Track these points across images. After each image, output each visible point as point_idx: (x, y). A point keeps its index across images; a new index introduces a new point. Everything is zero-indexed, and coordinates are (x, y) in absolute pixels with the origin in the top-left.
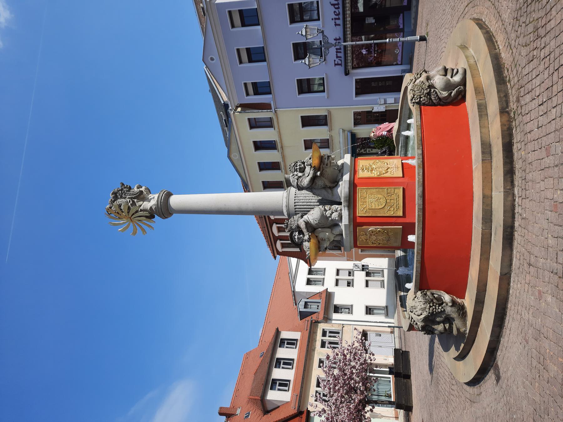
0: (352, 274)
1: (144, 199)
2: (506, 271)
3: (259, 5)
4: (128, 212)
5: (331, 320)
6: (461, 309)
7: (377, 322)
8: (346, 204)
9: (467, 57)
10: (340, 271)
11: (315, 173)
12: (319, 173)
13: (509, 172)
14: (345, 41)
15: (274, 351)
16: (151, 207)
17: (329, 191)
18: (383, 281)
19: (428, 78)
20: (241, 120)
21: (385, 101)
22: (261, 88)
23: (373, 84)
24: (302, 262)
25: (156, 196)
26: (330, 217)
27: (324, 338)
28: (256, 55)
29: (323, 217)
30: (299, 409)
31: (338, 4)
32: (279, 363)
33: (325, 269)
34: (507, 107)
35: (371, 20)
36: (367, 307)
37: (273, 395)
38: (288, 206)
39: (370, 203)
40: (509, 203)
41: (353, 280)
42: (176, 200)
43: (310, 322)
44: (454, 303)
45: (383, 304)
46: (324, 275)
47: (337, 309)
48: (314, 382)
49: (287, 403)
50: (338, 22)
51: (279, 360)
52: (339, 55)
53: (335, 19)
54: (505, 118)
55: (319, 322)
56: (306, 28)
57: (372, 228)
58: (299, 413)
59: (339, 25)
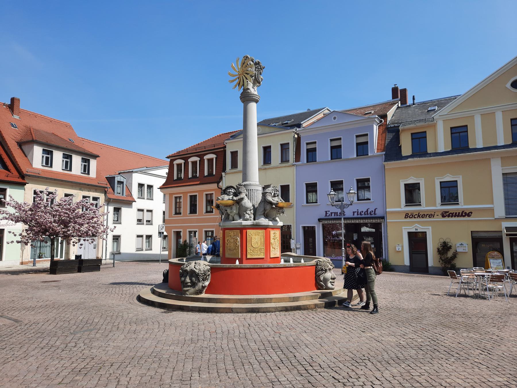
0: (148, 223)
1: (254, 84)
2: (234, 310)
3: (371, 157)
4: (246, 73)
5: (108, 205)
6: (200, 292)
7: (106, 245)
8: (255, 224)
9: (340, 290)
10: (150, 213)
11: (274, 204)
12: (274, 206)
13: (287, 309)
14: (344, 219)
15: (78, 153)
16: (249, 89)
17: (263, 213)
18: (142, 250)
19: (330, 269)
20: (288, 137)
21: (299, 248)
22: (312, 153)
23: (311, 240)
24: (164, 181)
25: (256, 93)
26: (246, 213)
27: (91, 198)
28: (336, 152)
29: (246, 209)
30: (27, 175)
31: (368, 214)
32: (68, 157)
33: (152, 200)
34: (318, 307)
35: (355, 237)
36: (119, 236)
37: (38, 151)
38: (250, 185)
39: (255, 238)
40: (271, 310)
41: (143, 224)
42: (253, 107)
43: (106, 186)
44: (203, 287)
45: (123, 250)
46: (147, 199)
47: (117, 210)
48: (51, 189)
49: (31, 165)
50: (356, 214)
51: (70, 157)
52: (333, 214)
53: (358, 212)
54: (313, 306)
55: (105, 194)
56: (354, 193)
57: (239, 239)
58: (22, 176)
59: (354, 215)
